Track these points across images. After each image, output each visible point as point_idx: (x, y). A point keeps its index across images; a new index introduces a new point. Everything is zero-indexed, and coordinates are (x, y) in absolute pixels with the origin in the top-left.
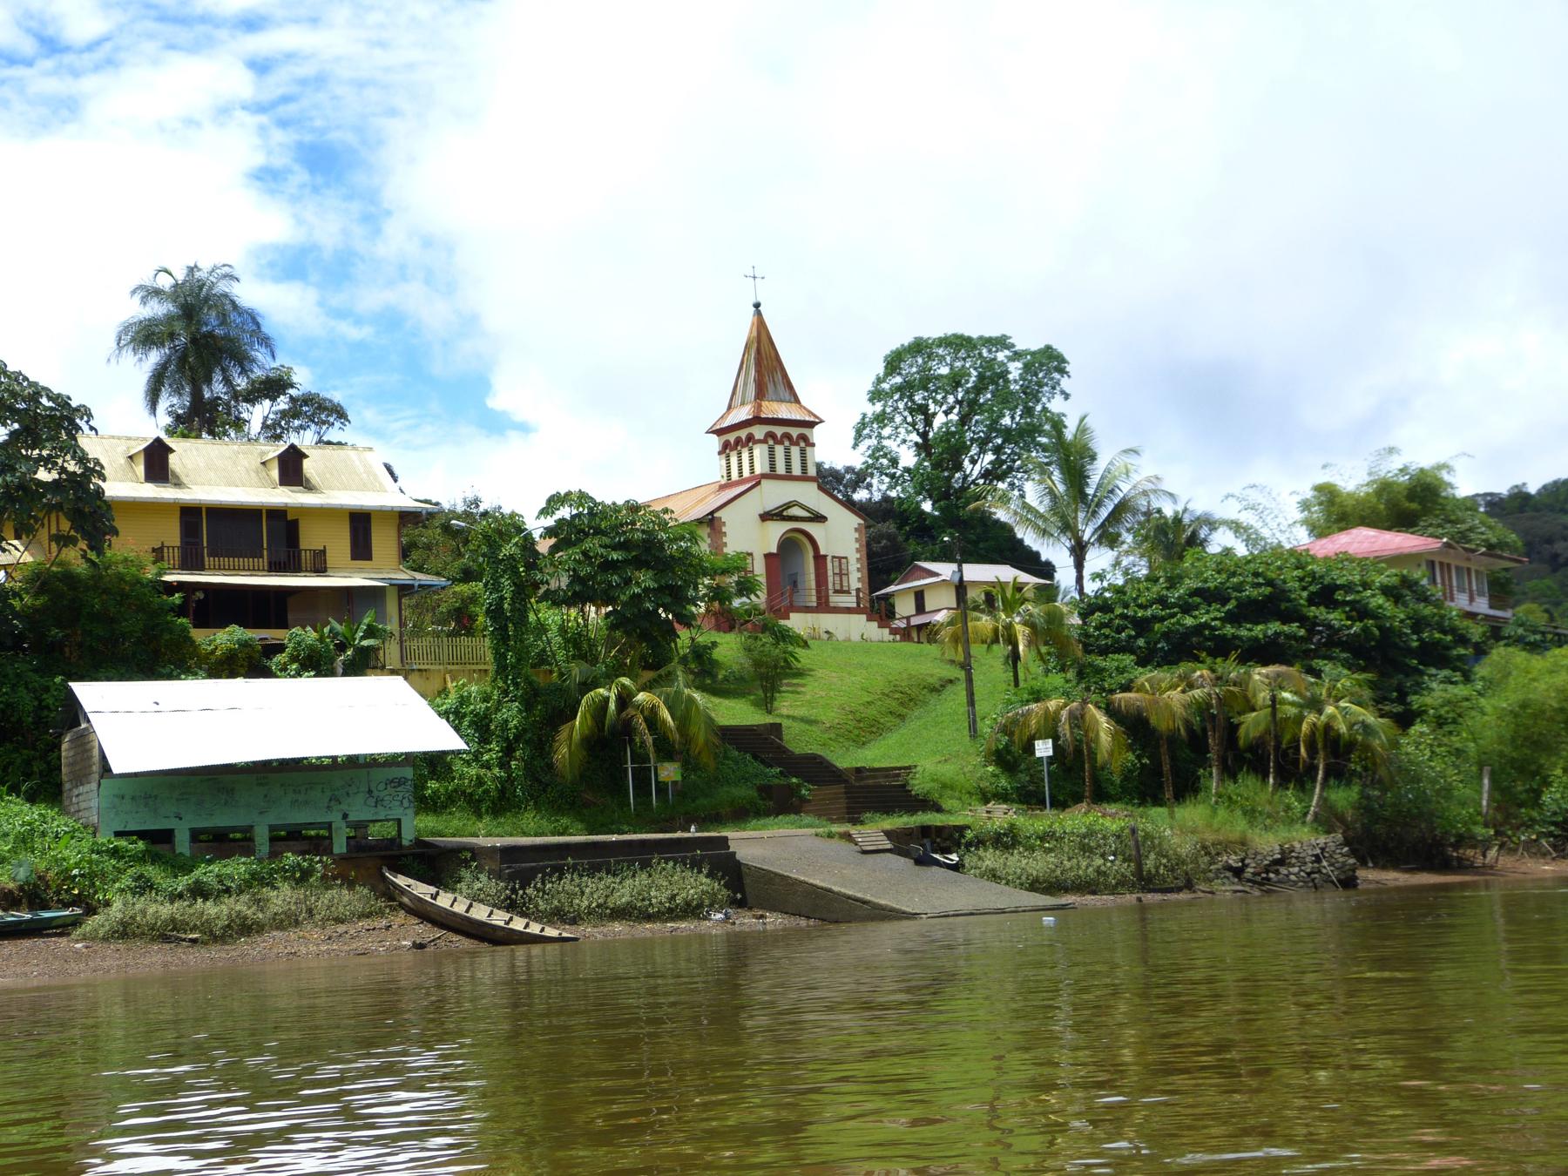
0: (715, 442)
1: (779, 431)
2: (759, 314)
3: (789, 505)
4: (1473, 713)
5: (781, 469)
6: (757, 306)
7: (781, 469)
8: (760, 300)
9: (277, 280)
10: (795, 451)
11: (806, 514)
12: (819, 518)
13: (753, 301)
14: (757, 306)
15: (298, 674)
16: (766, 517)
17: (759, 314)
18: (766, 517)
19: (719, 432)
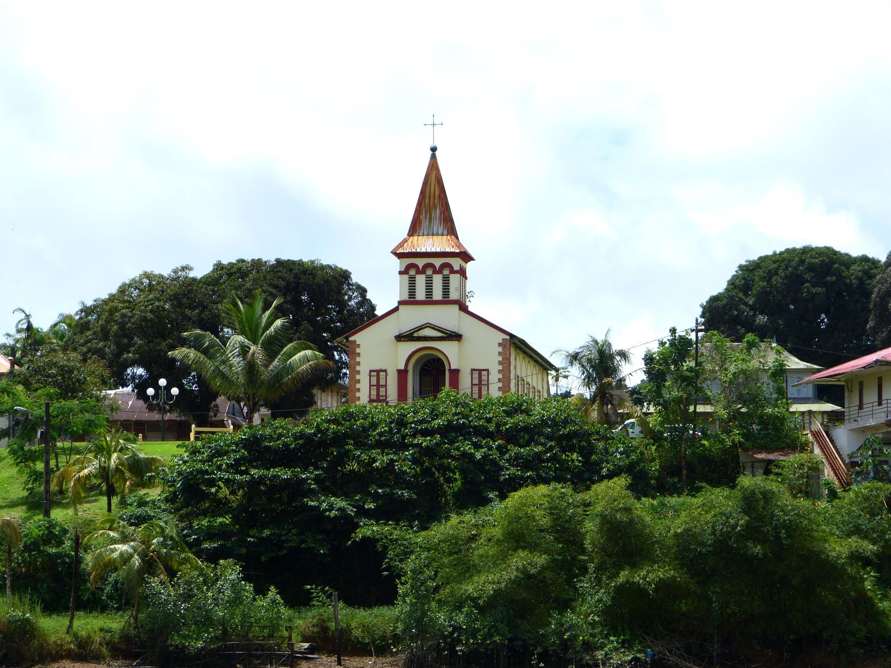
0: (397, 264)
1: (421, 262)
2: (433, 157)
3: (421, 328)
4: (596, 543)
5: (421, 295)
6: (434, 149)
7: (421, 295)
8: (436, 144)
9: (153, 460)
10: (437, 280)
11: (439, 334)
12: (455, 337)
13: (431, 145)
14: (434, 149)
15: (123, 290)
16: (400, 338)
17: (433, 157)
18: (400, 338)
19: (400, 256)
